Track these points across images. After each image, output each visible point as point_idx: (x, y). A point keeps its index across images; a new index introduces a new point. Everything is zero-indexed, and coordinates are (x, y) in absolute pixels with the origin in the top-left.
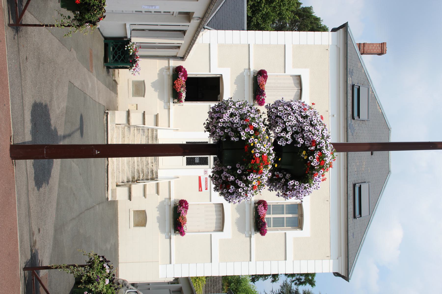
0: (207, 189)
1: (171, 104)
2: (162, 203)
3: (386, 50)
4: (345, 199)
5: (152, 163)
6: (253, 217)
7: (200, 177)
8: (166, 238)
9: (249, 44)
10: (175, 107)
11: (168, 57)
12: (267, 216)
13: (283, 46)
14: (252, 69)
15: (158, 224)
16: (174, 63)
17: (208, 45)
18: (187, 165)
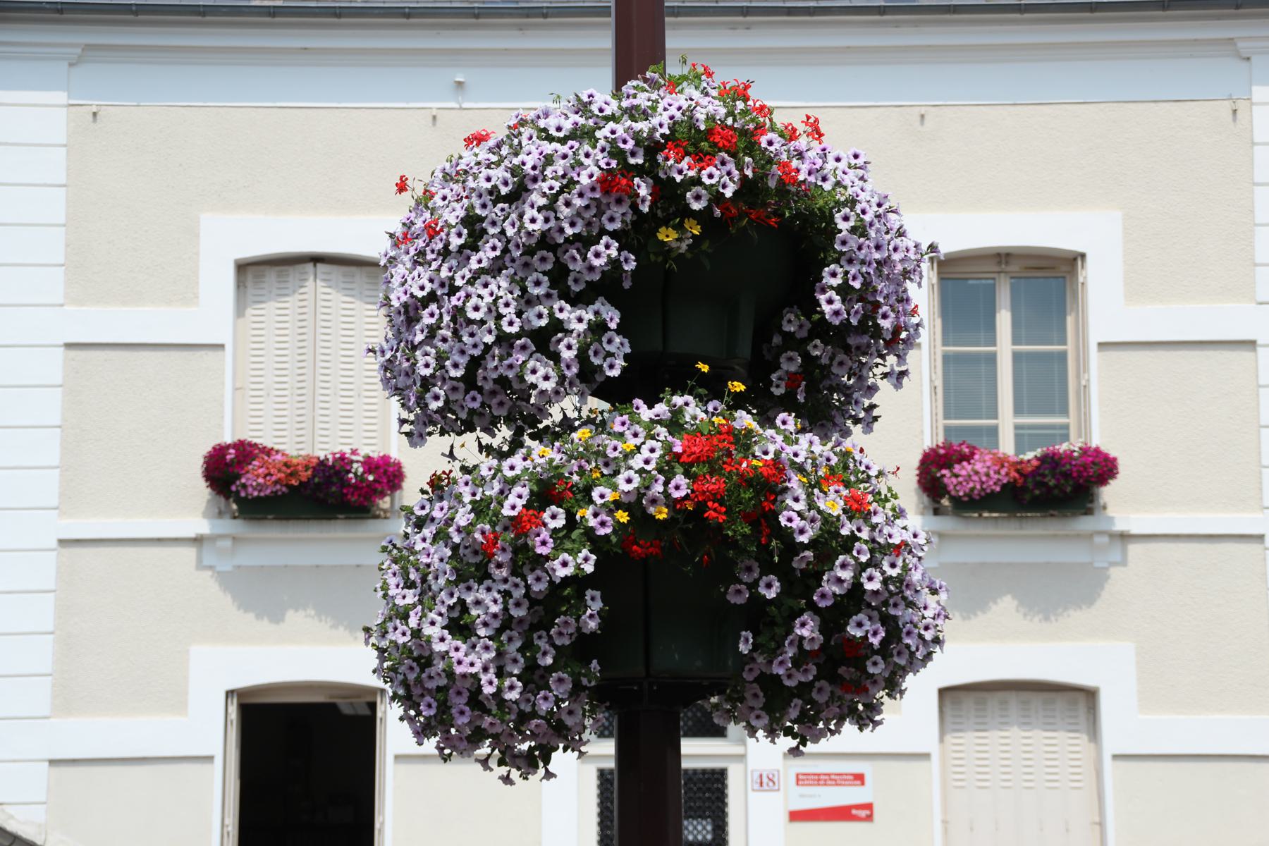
0: (859, 778)
4: (916, 24)
7: (796, 816)
9: (63, 542)
12: (1007, 446)
13: (73, 353)
14: (200, 525)
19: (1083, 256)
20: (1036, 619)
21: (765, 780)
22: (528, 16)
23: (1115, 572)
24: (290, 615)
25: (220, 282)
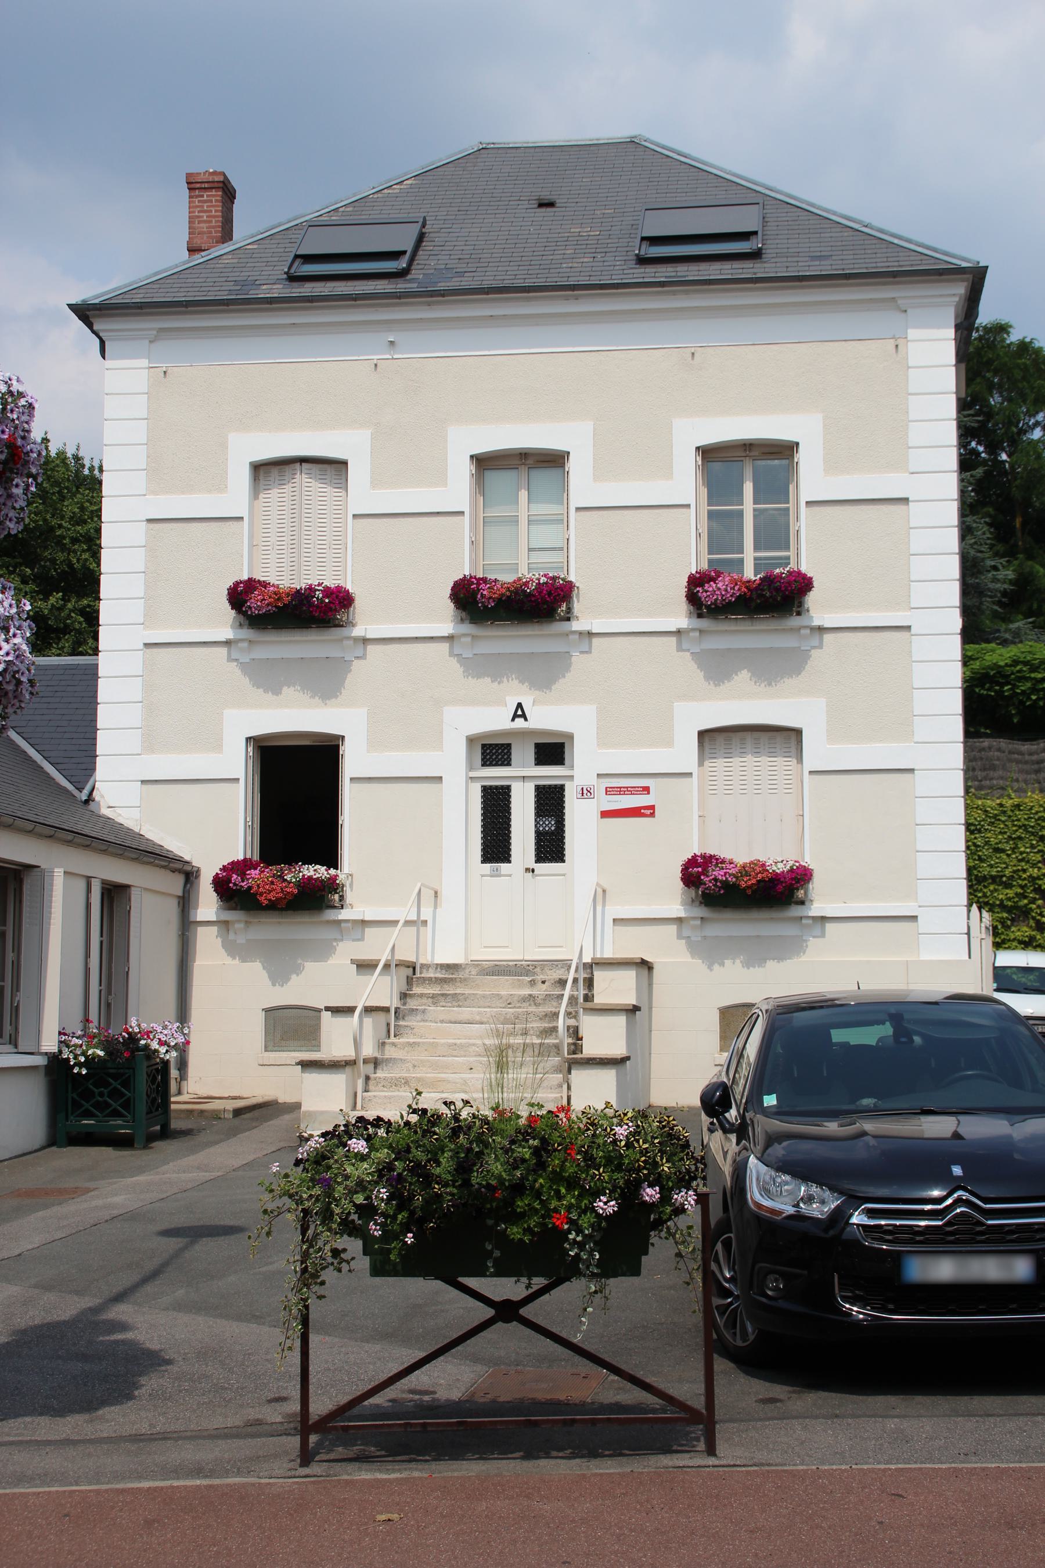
0: (646, 790)
1: (344, 915)
2: (695, 949)
3: (215, 173)
4: (687, 292)
5: (533, 983)
6: (748, 622)
7: (605, 814)
8: (823, 936)
9: (146, 645)
10: (357, 905)
11: (186, 926)
12: (749, 573)
13: (152, 526)
14: (227, 632)
15: (771, 964)
16: (208, 905)
17: (146, 787)
18: (509, 862)
19: (797, 444)
20: (763, 685)
21: (585, 792)
22: (432, 296)
23: (814, 653)
24: (285, 689)
25: (241, 478)
